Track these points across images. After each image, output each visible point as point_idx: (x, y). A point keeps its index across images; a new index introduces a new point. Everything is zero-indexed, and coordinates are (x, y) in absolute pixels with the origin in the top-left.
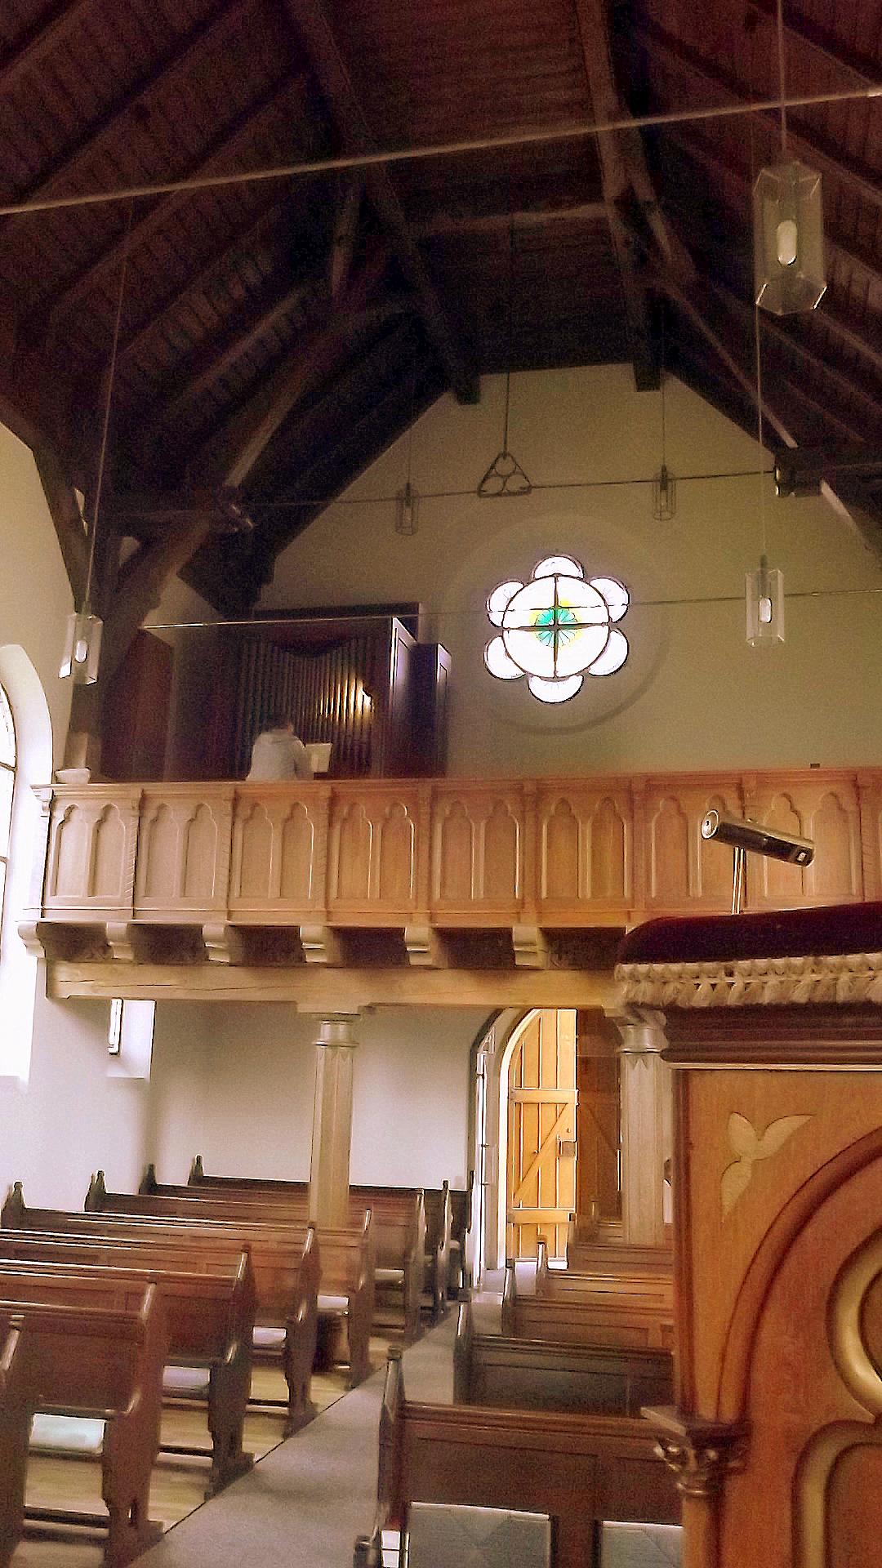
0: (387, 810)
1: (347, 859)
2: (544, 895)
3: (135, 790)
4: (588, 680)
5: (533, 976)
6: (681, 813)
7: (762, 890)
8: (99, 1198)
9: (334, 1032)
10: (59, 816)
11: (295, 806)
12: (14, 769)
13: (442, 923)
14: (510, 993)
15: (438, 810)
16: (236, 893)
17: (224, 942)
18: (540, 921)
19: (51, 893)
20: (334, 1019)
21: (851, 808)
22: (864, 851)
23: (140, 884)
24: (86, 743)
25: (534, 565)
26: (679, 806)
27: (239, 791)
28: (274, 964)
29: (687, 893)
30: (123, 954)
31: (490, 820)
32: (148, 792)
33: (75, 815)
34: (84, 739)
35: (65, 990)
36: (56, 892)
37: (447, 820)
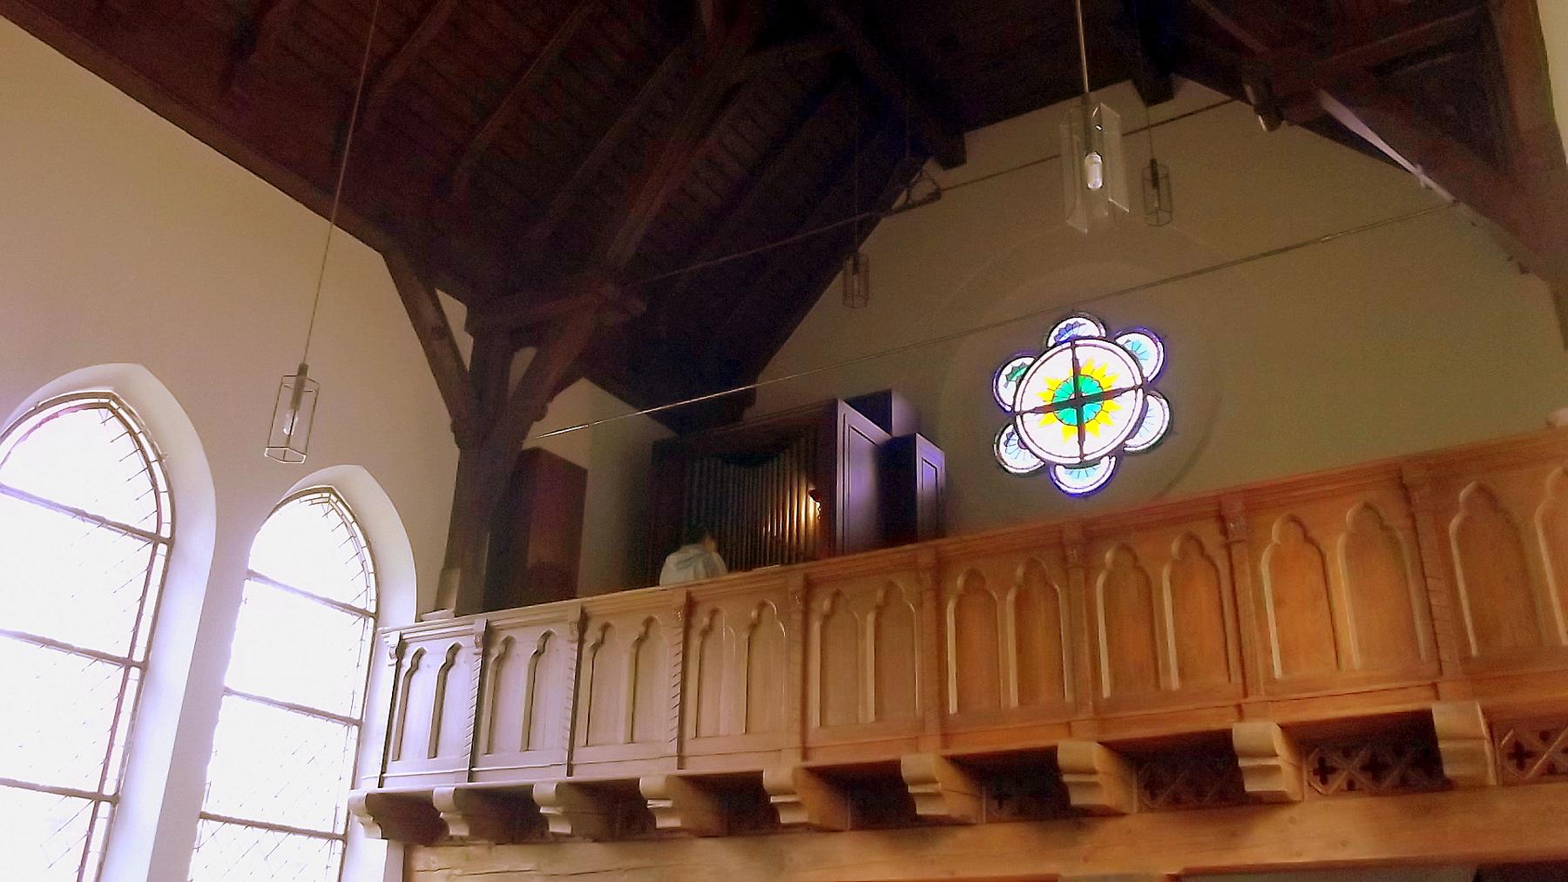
0: (754, 614)
1: (707, 680)
2: (953, 707)
3: (479, 623)
5: (963, 834)
7: (1270, 668)
10: (407, 663)
11: (649, 622)
12: (376, 616)
13: (819, 760)
14: (933, 862)
15: (814, 605)
16: (580, 740)
17: (559, 805)
18: (945, 745)
21: (1395, 516)
22: (1430, 587)
24: (459, 575)
25: (998, 404)
26: (1135, 558)
28: (644, 836)
30: (458, 830)
31: (880, 611)
33: (461, 657)
34: (456, 577)
36: (436, 752)
37: (826, 618)
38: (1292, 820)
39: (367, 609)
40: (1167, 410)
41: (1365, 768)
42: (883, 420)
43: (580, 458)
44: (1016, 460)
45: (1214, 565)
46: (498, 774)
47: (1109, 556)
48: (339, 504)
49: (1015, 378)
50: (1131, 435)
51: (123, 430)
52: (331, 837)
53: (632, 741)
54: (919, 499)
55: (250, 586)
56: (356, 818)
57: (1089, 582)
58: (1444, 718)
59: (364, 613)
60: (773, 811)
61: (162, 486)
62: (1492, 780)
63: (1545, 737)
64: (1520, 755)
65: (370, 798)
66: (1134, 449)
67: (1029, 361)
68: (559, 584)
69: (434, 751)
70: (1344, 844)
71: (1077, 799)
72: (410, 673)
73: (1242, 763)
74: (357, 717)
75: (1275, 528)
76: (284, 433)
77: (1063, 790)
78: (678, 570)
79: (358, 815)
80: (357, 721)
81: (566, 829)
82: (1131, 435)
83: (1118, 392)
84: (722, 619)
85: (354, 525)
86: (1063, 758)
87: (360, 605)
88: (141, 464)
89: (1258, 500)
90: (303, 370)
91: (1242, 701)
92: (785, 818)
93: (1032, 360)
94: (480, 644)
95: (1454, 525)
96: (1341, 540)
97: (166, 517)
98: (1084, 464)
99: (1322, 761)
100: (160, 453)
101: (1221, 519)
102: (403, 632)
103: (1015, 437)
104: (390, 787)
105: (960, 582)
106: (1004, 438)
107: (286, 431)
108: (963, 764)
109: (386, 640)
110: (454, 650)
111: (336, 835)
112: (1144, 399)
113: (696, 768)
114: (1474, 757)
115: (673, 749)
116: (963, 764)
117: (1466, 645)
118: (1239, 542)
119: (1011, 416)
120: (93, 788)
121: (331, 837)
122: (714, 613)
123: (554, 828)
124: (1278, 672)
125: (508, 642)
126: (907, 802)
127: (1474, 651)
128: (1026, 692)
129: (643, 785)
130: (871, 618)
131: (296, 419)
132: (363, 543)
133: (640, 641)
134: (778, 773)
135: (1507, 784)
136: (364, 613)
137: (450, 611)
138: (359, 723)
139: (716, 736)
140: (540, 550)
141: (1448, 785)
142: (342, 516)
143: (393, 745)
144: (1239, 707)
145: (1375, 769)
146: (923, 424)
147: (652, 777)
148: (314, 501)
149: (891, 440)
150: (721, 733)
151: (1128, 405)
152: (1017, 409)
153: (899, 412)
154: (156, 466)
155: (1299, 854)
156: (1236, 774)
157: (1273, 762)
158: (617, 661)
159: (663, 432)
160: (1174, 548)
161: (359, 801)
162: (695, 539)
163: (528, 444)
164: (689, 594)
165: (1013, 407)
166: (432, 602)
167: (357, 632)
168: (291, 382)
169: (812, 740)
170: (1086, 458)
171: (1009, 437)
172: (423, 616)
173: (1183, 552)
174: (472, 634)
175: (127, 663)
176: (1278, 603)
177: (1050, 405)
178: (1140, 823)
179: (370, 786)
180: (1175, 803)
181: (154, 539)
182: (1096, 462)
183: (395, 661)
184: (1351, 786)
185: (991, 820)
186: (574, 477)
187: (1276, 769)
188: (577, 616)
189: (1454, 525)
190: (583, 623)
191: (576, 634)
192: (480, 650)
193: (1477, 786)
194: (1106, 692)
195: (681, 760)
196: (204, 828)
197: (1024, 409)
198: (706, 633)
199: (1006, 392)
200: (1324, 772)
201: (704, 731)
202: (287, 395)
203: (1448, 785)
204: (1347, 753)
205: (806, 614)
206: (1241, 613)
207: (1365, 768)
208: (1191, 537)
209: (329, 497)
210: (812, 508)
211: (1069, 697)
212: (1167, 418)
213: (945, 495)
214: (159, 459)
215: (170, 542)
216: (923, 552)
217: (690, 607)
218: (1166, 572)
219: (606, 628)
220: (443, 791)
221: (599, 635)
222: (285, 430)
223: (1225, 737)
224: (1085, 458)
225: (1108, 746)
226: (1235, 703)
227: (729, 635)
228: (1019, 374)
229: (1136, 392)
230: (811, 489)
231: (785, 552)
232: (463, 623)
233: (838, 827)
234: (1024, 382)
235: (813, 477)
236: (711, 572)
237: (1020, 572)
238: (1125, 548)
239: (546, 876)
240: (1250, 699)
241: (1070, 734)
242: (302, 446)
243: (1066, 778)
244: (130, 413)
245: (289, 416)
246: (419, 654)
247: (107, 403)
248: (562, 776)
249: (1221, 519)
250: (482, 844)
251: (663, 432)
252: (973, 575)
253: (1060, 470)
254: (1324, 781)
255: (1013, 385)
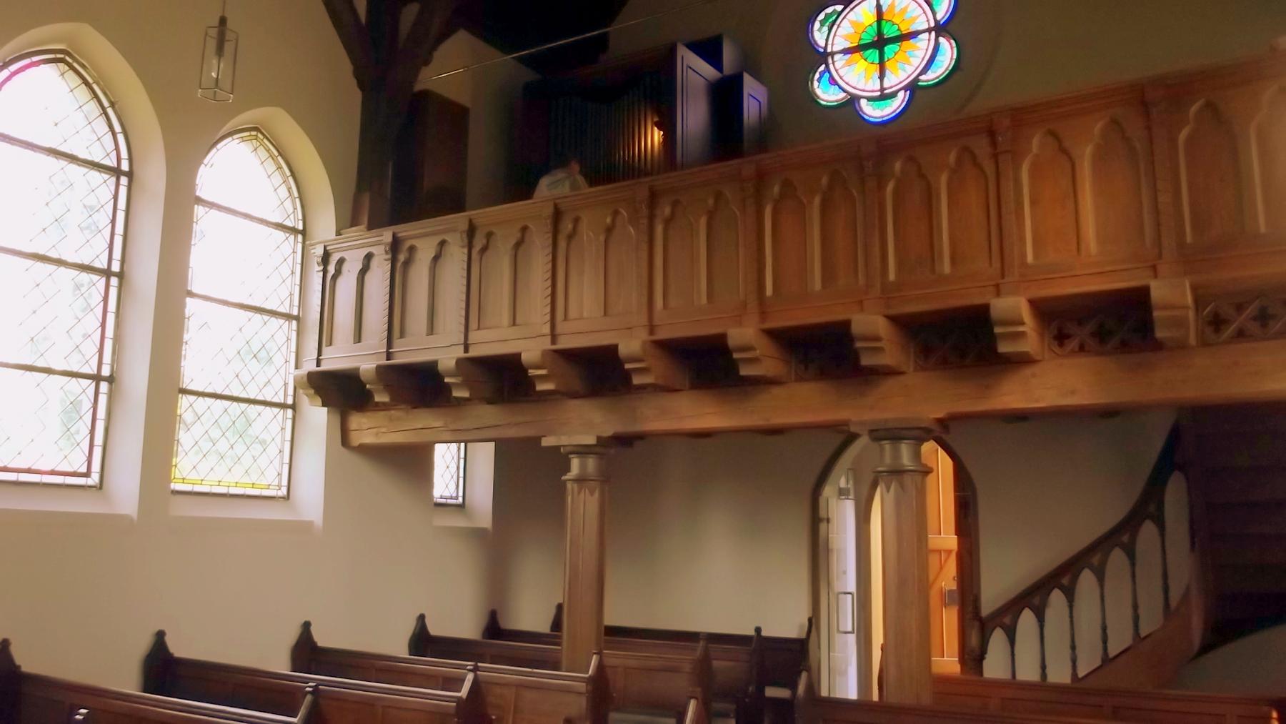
0: (609, 220)
2: (769, 291)
3: (387, 235)
4: (918, 93)
5: (776, 391)
6: (922, 176)
7: (1024, 255)
8: (423, 641)
9: (583, 466)
10: (331, 269)
11: (524, 229)
13: (662, 335)
16: (473, 323)
17: (459, 376)
19: (326, 342)
20: (583, 451)
23: (395, 327)
25: (812, 45)
27: (474, 221)
29: (933, 271)
30: (382, 397)
32: (400, 235)
33: (375, 263)
34: (366, 200)
35: (359, 438)
37: (668, 222)
38: (1034, 375)
39: (296, 227)
40: (955, 50)
41: (1093, 335)
42: (715, 61)
43: (468, 105)
44: (827, 94)
45: (983, 171)
46: (411, 352)
47: (898, 166)
48: (265, 140)
49: (827, 24)
50: (924, 71)
51: (79, 81)
52: (283, 406)
53: (514, 324)
54: (746, 132)
55: (199, 210)
56: (301, 391)
57: (881, 187)
58: (1159, 291)
59: (293, 230)
60: (627, 375)
61: (118, 128)
62: (1192, 340)
63: (1240, 308)
64: (1217, 322)
65: (311, 375)
66: (925, 84)
67: (839, 8)
68: (451, 202)
69: (358, 337)
70: (1073, 393)
71: (866, 361)
72: (335, 277)
73: (997, 330)
74: (295, 312)
75: (1035, 142)
76: (212, 76)
77: (856, 355)
78: (551, 188)
79: (303, 389)
80: (296, 316)
81: (465, 394)
82: (924, 71)
83: (913, 35)
84: (584, 226)
85: (279, 158)
86: (856, 329)
87: (289, 223)
88: (98, 111)
89: (1022, 117)
90: (223, 21)
91: (1001, 281)
92: (637, 380)
93: (842, 7)
94: (389, 252)
95: (1183, 135)
96: (1089, 150)
97: (124, 154)
98: (884, 96)
99: (1060, 330)
100: (113, 100)
101: (992, 134)
102: (326, 244)
103: (827, 75)
104: (324, 367)
105: (776, 189)
106: (817, 76)
107: (214, 75)
108: (775, 335)
109: (313, 251)
110: (369, 257)
111: (286, 404)
112: (936, 40)
113: (565, 343)
114: (1180, 323)
115: (546, 329)
116: (775, 335)
117: (1181, 233)
118: (1006, 152)
119: (823, 57)
120: (91, 369)
121: (283, 406)
122: (576, 221)
123: (457, 393)
124: (1030, 258)
125: (412, 249)
126: (732, 366)
127: (1189, 239)
128: (829, 274)
129: (525, 358)
130: (703, 221)
131: (222, 65)
132: (288, 173)
133: (518, 245)
134: (630, 346)
135: (1204, 343)
136: (293, 230)
137: (363, 227)
138: (297, 318)
139: (581, 318)
140: (432, 177)
141: (1158, 346)
142: (268, 150)
143: (325, 335)
144: (997, 286)
145: (1102, 336)
146: (750, 64)
147: (531, 350)
148: (245, 139)
149: (722, 78)
150: (585, 315)
151: (923, 44)
152: (829, 50)
153: (729, 55)
154: (110, 111)
155: (1037, 401)
156: (992, 339)
157: (1021, 329)
158: (500, 264)
159: (529, 75)
160: (952, 158)
161: (302, 378)
162: (562, 163)
163: (418, 87)
164: (556, 206)
165: (825, 48)
166: (349, 219)
167: (288, 246)
168: (214, 32)
169: (656, 321)
170: (886, 92)
171: (822, 74)
172: (342, 231)
173: (959, 162)
174: (382, 244)
175: (107, 273)
176: (1034, 203)
177: (857, 46)
178: (913, 379)
179: (310, 366)
180: (944, 364)
181: (116, 172)
182: (894, 95)
183: (321, 268)
184: (1082, 348)
185: (800, 379)
186: (456, 116)
187: (1022, 334)
188: (465, 226)
189: (1183, 135)
190: (471, 231)
191: (466, 241)
192: (389, 256)
193: (1182, 346)
194: (892, 276)
195: (554, 337)
196: (184, 401)
197: (835, 50)
198: (570, 237)
199: (819, 36)
200: (1061, 338)
201: (573, 313)
202: (212, 45)
203: (1158, 346)
204: (1080, 323)
205: (651, 218)
206: (1004, 210)
207: (1093, 335)
208: (966, 149)
209: (257, 136)
210: (656, 136)
211: (861, 280)
212: (955, 57)
213: (769, 125)
214: (112, 105)
215: (130, 175)
216: (746, 166)
217: (557, 216)
218: (944, 179)
219: (489, 235)
220: (367, 366)
221: (484, 241)
222: (213, 74)
223: (984, 310)
224: (886, 92)
225: (894, 319)
226: (993, 283)
227: (590, 236)
228: (831, 20)
229: (930, 34)
230: (656, 119)
231: (633, 171)
232: (372, 237)
233: (678, 387)
234: (835, 27)
235: (658, 111)
236: (574, 187)
237: (825, 180)
238: (911, 159)
239: (452, 431)
240: (1007, 279)
241: (862, 310)
242: (228, 87)
243: (858, 345)
244: (83, 66)
245: (215, 62)
246: (341, 262)
247: (61, 57)
248: (460, 353)
249: (992, 134)
250: (401, 409)
251: (529, 75)
252: (787, 184)
253: (863, 102)
254: (1061, 345)
255: (825, 29)
